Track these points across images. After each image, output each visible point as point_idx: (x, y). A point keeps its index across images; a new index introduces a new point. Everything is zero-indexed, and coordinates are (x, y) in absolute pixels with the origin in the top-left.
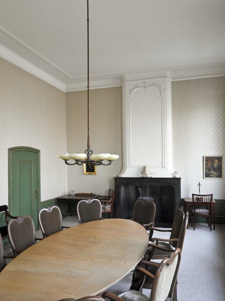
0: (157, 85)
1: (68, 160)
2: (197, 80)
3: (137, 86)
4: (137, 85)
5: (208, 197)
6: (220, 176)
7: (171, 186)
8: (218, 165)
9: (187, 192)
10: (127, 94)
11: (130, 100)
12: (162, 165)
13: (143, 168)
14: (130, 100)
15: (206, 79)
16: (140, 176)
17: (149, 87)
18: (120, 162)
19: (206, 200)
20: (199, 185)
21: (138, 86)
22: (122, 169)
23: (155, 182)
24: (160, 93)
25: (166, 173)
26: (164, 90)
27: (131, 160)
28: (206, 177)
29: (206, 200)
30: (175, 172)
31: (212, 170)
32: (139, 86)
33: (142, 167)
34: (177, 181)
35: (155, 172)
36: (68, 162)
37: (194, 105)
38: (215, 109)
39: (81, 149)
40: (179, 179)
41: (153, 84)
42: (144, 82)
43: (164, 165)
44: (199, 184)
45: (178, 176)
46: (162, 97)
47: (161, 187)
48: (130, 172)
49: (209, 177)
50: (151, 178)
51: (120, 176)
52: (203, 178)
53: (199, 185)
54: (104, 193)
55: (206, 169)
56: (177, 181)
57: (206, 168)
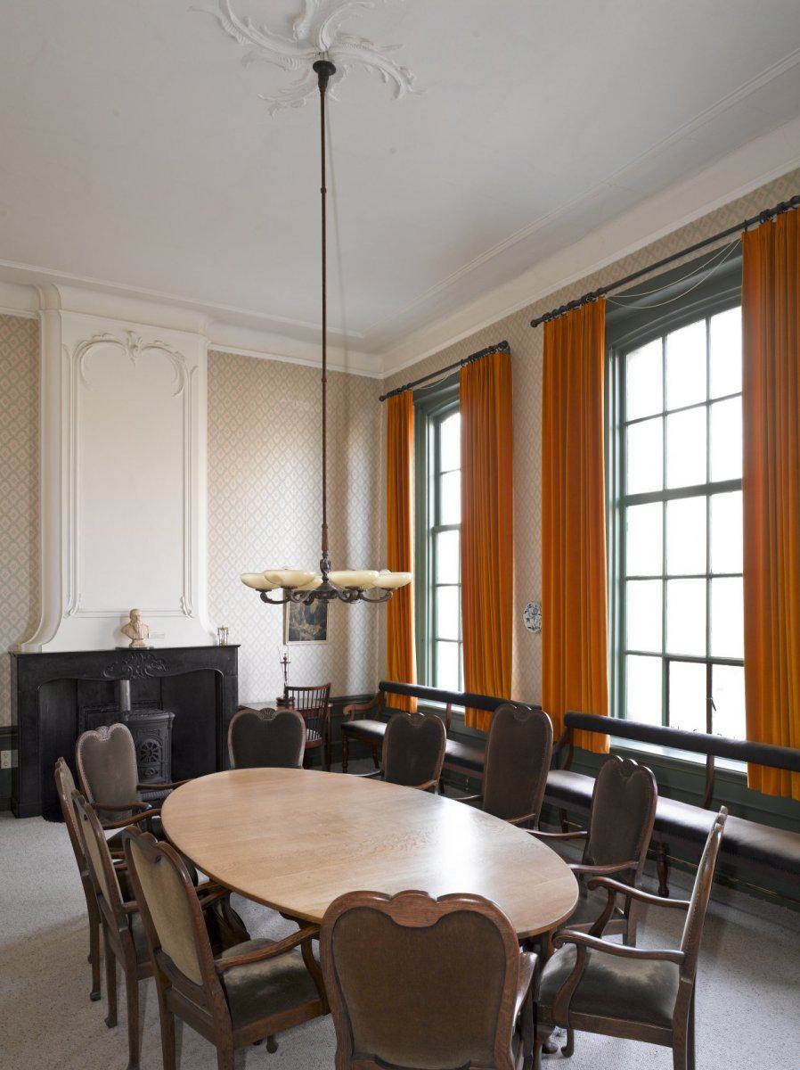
0: (170, 349)
1: (270, 590)
2: (273, 364)
3: (104, 339)
4: (105, 334)
5: (315, 692)
6: (322, 636)
7: (210, 670)
8: (318, 606)
9: (259, 686)
10: (67, 354)
11: (79, 380)
12: (182, 608)
13: (122, 617)
14: (79, 380)
15: (296, 367)
16: (110, 645)
17: (146, 351)
18: (22, 597)
19: (301, 702)
20: (285, 663)
21: (107, 337)
22: (35, 623)
23: (164, 662)
24: (178, 380)
25: (197, 634)
26: (191, 373)
27: (78, 592)
28: (291, 639)
29: (301, 702)
30: (223, 629)
31: (305, 621)
32: (112, 337)
33: (119, 614)
34: (227, 654)
35: (162, 634)
36: (269, 595)
37: (265, 432)
38: (303, 452)
39: (230, 554)
40: (232, 650)
41: (158, 343)
42: (130, 332)
43: (189, 608)
44: (285, 659)
45: (230, 641)
46: (184, 394)
47: (161, 679)
48: (72, 634)
49: (298, 640)
50: (152, 650)
51: (35, 649)
52: (284, 643)
53: (285, 663)
54: (10, 721)
55: (291, 619)
56: (227, 654)
57: (291, 614)
